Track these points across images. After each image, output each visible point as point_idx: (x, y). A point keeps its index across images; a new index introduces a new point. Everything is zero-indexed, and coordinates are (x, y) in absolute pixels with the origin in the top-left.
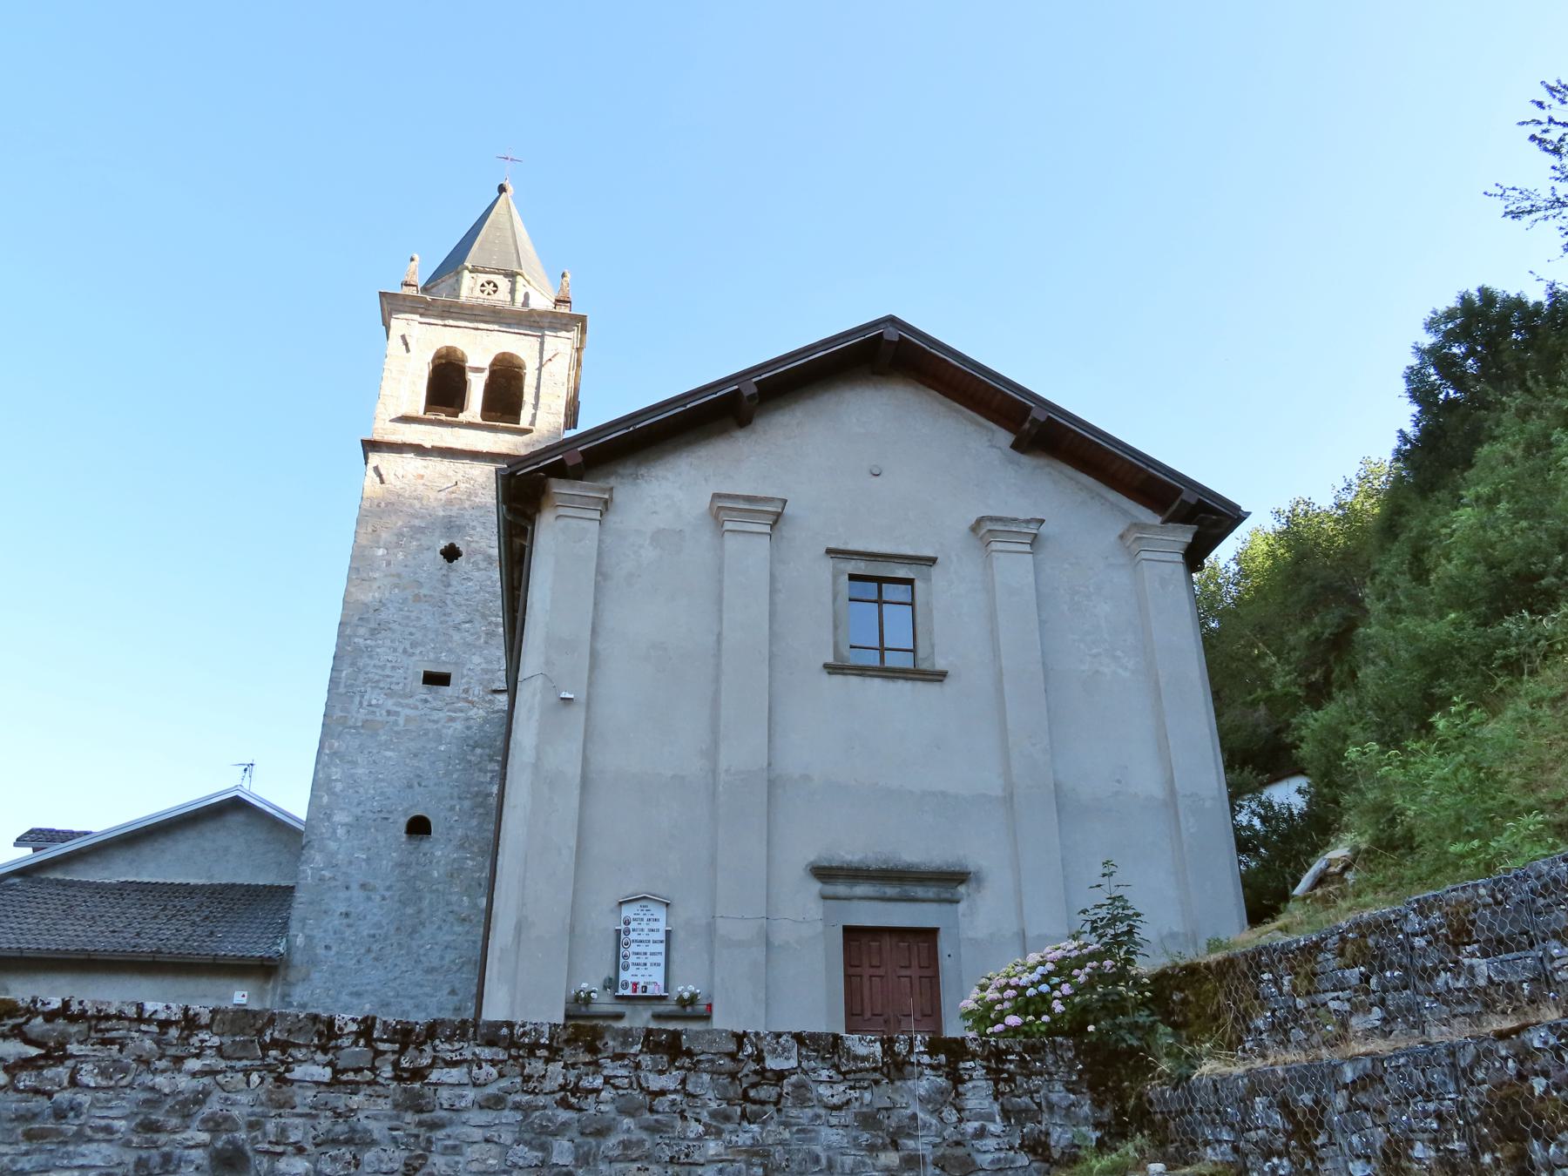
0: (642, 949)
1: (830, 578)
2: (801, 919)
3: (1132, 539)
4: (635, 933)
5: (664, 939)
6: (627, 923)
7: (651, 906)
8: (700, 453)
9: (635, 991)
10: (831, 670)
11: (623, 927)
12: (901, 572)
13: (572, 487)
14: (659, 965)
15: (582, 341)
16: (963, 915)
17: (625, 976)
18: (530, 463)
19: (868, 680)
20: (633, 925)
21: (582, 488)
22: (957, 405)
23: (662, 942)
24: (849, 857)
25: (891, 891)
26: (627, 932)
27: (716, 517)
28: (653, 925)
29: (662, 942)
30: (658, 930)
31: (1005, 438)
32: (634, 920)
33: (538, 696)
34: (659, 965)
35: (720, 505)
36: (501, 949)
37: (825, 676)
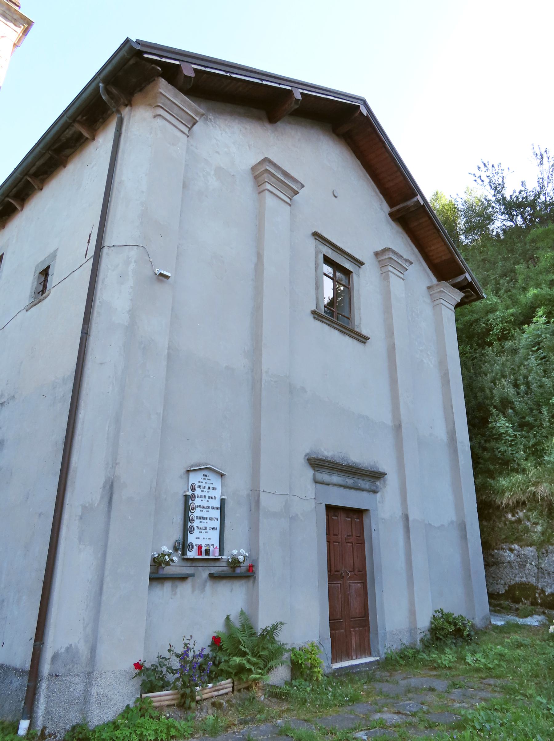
0: (204, 514)
1: (314, 252)
2: (303, 497)
3: (439, 290)
4: (199, 499)
5: (219, 506)
6: (193, 489)
7: (211, 476)
8: (246, 126)
9: (200, 553)
10: (316, 316)
11: (190, 493)
12: (347, 265)
13: (176, 96)
14: (215, 529)
15: (20, 40)
16: (379, 502)
17: (191, 539)
18: (155, 52)
19: (333, 330)
20: (198, 492)
21: (183, 101)
22: (368, 175)
23: (218, 508)
24: (326, 453)
25: (350, 481)
26: (193, 496)
27: (256, 178)
28: (212, 493)
29: (218, 508)
30: (215, 498)
31: (387, 209)
32: (199, 487)
33: (132, 266)
34: (215, 529)
35: (268, 168)
36: (84, 507)
37: (311, 318)
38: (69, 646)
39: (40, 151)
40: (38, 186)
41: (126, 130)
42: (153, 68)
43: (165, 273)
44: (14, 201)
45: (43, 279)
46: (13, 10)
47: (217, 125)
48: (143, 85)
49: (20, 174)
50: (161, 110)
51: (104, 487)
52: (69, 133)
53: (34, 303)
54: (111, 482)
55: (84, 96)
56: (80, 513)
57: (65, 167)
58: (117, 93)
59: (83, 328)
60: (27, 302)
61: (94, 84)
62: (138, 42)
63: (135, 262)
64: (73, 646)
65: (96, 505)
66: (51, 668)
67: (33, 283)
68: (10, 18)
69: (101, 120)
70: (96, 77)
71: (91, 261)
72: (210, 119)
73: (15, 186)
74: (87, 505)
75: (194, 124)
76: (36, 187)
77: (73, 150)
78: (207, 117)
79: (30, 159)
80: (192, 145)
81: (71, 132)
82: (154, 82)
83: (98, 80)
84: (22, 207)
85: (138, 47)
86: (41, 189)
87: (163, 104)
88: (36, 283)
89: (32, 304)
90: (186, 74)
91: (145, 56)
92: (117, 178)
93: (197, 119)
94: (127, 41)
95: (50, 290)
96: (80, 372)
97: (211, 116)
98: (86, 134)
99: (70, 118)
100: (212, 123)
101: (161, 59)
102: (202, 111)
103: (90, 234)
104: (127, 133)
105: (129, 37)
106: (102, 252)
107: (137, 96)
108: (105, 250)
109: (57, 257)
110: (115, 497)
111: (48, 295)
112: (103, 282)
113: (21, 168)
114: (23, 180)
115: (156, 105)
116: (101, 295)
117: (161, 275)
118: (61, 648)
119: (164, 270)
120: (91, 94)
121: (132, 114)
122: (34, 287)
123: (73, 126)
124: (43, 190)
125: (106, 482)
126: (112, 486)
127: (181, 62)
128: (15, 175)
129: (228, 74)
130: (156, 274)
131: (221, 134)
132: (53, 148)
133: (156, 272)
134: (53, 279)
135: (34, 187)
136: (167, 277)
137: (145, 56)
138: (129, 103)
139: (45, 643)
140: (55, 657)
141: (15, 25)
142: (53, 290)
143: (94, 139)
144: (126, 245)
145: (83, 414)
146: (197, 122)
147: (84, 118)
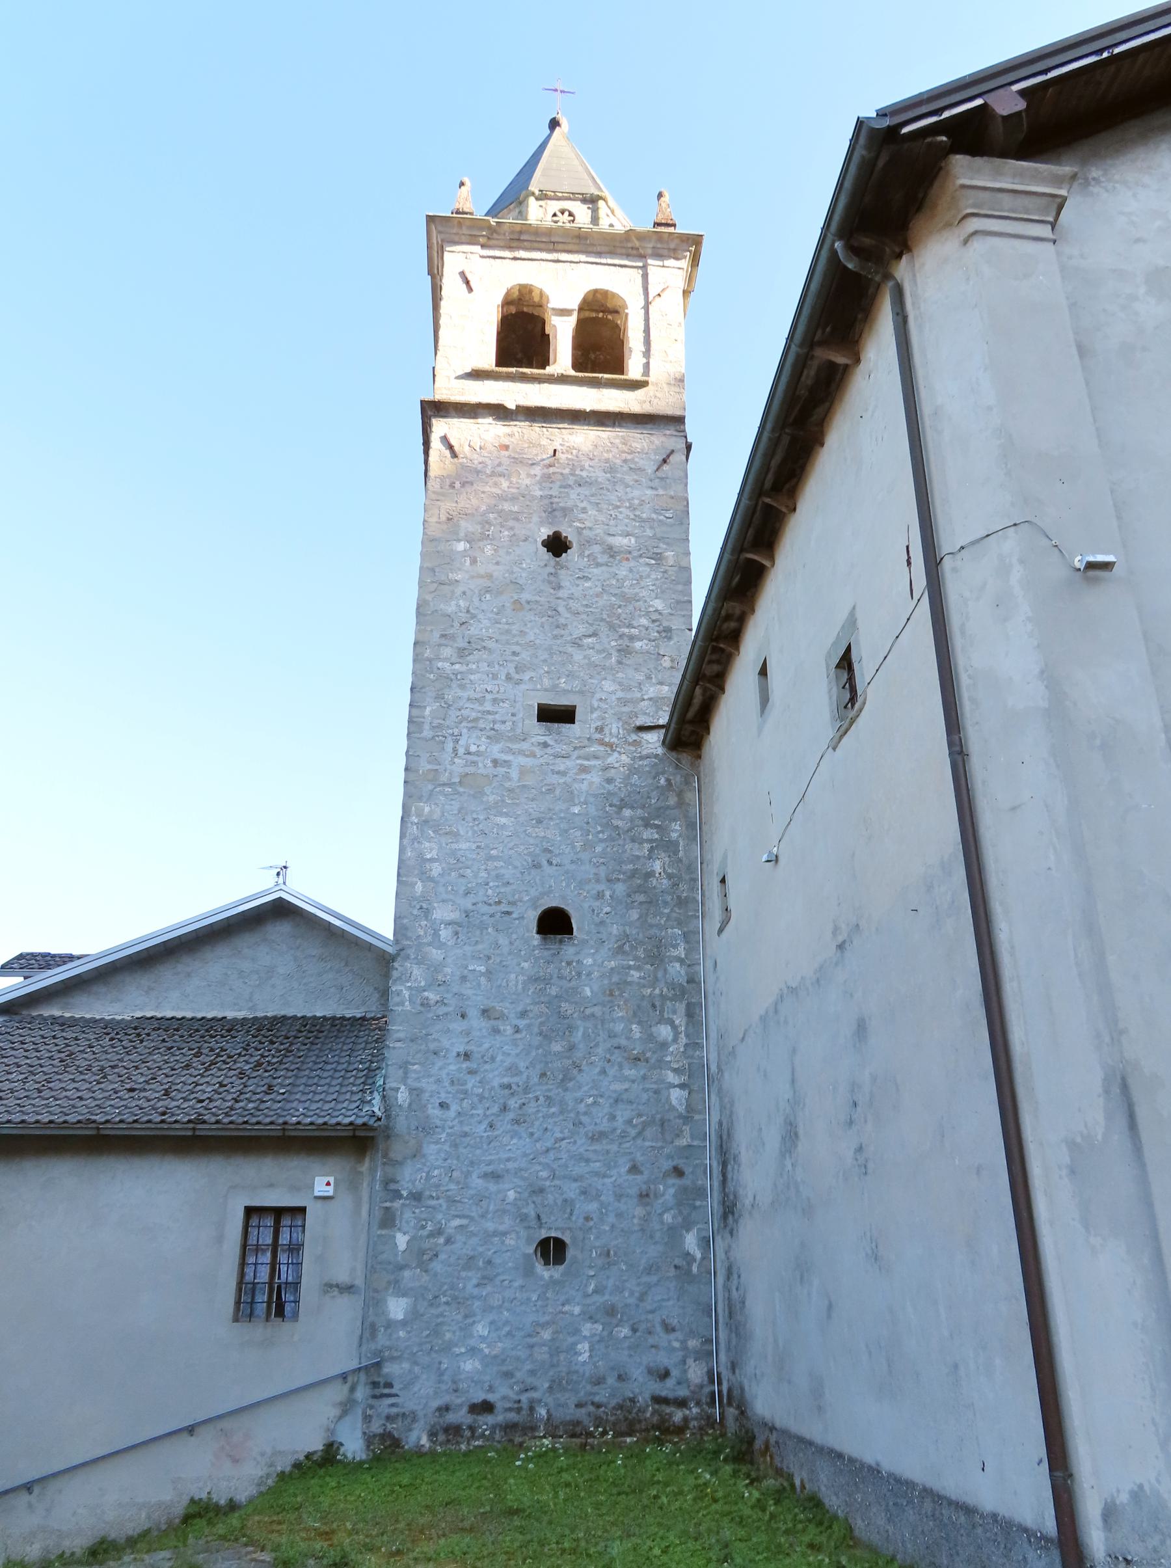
13: (998, 173)
21: (1020, 175)
33: (1017, 573)
36: (1072, 1145)
38: (1136, 1488)
39: (770, 439)
40: (787, 507)
41: (913, 304)
42: (930, 144)
43: (1100, 558)
44: (756, 554)
45: (845, 676)
46: (666, 236)
47: (1117, 182)
48: (920, 195)
49: (750, 499)
50: (975, 220)
51: (1107, 1092)
52: (809, 376)
53: (843, 729)
54: (1119, 1077)
55: (814, 286)
56: (1067, 1160)
57: (822, 445)
58: (873, 242)
59: (950, 744)
60: (830, 733)
61: (824, 253)
62: (882, 114)
63: (1021, 561)
64: (1147, 1488)
65: (1100, 1137)
66: (1107, 1539)
67: (830, 691)
68: (665, 252)
69: (860, 316)
70: (825, 236)
71: (926, 599)
72: (1094, 179)
73: (749, 526)
74: (1079, 1140)
75: (1060, 207)
76: (784, 510)
77: (827, 404)
78: (1086, 179)
79: (757, 464)
80: (1070, 258)
81: (813, 373)
82: (942, 173)
83: (830, 237)
84: (772, 558)
85: (886, 122)
86: (795, 509)
87: (974, 206)
88: (835, 689)
89: (839, 733)
90: (1005, 113)
91: (905, 130)
92: (926, 409)
93: (1063, 192)
94: (860, 123)
95: (865, 692)
96: (973, 849)
97: (1095, 173)
98: (840, 360)
99: (801, 345)
100: (1103, 185)
101: (941, 115)
102: (1066, 169)
103: (908, 547)
104: (919, 308)
105: (862, 115)
106: (942, 570)
107: (918, 225)
108: (947, 564)
109: (860, 623)
110: (1142, 1113)
111: (864, 703)
112: (963, 633)
113: (748, 488)
114: (759, 508)
115: (960, 217)
116: (966, 661)
117: (1091, 566)
118: (1118, 1491)
119: (1093, 554)
120: (825, 275)
121: (917, 266)
122: (835, 698)
123: (813, 357)
124: (798, 510)
125: (1107, 1081)
126: (1125, 1087)
127: (985, 96)
128: (742, 505)
129: (1105, 55)
130: (1080, 569)
131: (1134, 195)
132: (791, 420)
133: (1077, 565)
134: (864, 669)
135: (782, 512)
136: (1106, 566)
137: (905, 130)
138: (904, 247)
139: (1076, 1476)
140: (1109, 1514)
141: (677, 259)
142: (869, 691)
143: (858, 361)
144: (988, 536)
145: (1004, 932)
146: (1065, 199)
147: (828, 329)
